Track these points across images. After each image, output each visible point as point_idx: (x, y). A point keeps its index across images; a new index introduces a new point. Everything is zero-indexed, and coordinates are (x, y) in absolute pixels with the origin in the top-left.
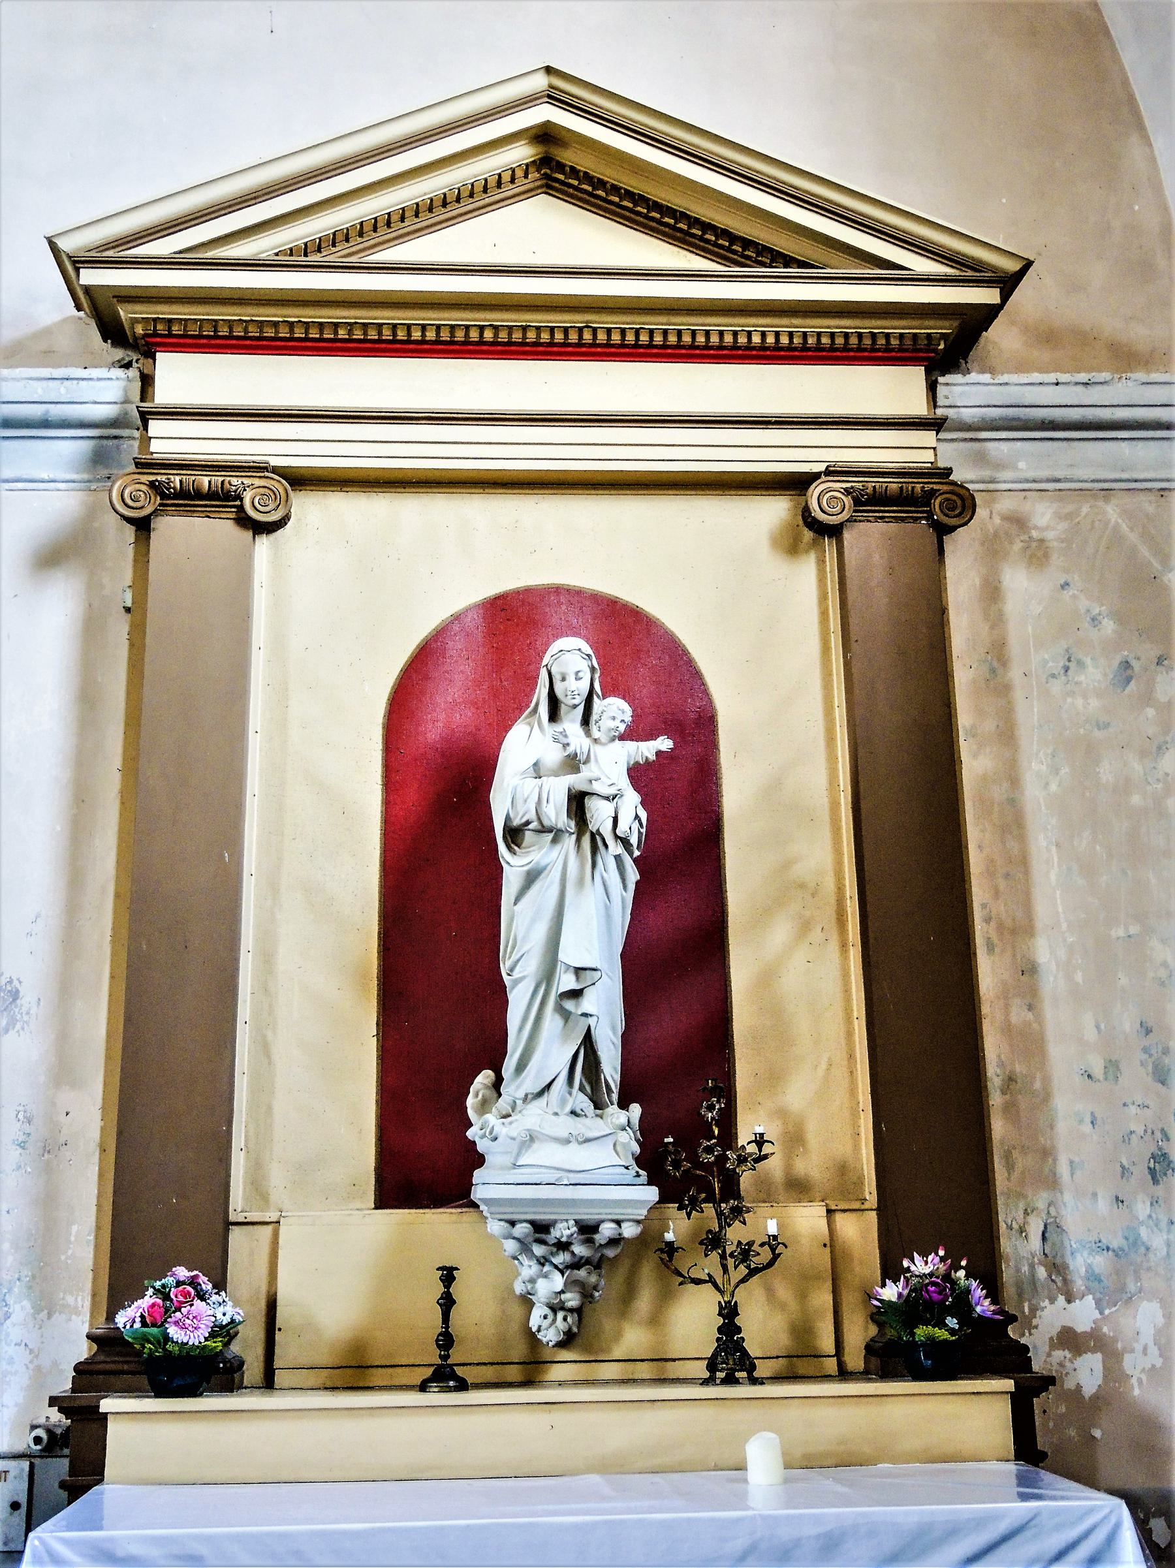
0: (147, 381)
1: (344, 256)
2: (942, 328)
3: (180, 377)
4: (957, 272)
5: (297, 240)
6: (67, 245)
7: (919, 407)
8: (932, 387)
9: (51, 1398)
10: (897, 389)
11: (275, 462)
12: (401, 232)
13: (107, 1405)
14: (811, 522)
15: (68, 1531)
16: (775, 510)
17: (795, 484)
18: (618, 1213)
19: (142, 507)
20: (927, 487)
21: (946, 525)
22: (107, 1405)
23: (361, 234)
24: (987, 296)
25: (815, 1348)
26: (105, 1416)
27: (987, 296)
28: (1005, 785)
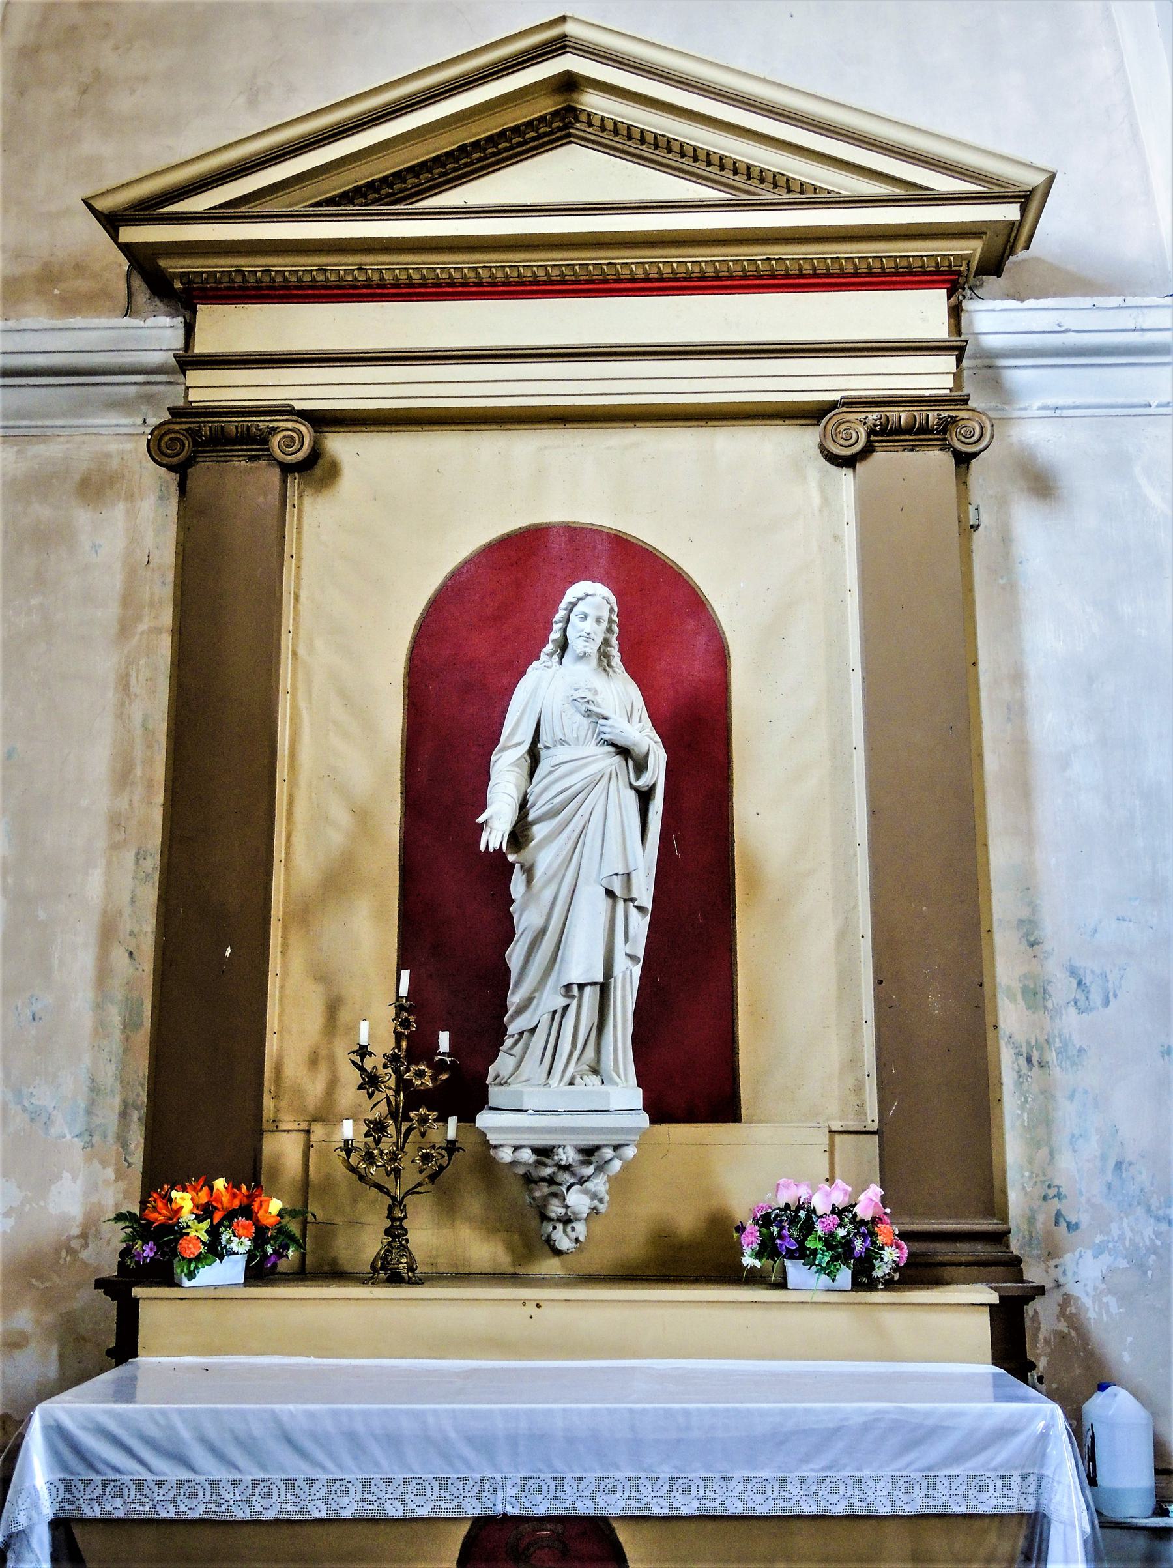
0: (189, 330)
1: (311, 206)
2: (973, 248)
3: (226, 327)
4: (903, 192)
5: (772, 166)
6: (102, 205)
7: (940, 330)
8: (955, 312)
9: (97, 1280)
10: (922, 312)
11: (298, 406)
12: (660, 159)
13: (137, 1292)
14: (287, 469)
15: (116, 1402)
16: (807, 438)
17: (813, 414)
18: (617, 1139)
19: (982, 428)
20: (944, 414)
21: (967, 454)
22: (137, 1292)
23: (709, 163)
24: (1011, 212)
25: (334, 1261)
26: (137, 1300)
27: (1011, 212)
28: (150, 727)
